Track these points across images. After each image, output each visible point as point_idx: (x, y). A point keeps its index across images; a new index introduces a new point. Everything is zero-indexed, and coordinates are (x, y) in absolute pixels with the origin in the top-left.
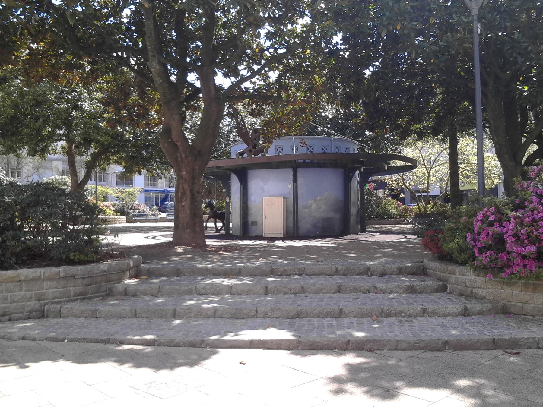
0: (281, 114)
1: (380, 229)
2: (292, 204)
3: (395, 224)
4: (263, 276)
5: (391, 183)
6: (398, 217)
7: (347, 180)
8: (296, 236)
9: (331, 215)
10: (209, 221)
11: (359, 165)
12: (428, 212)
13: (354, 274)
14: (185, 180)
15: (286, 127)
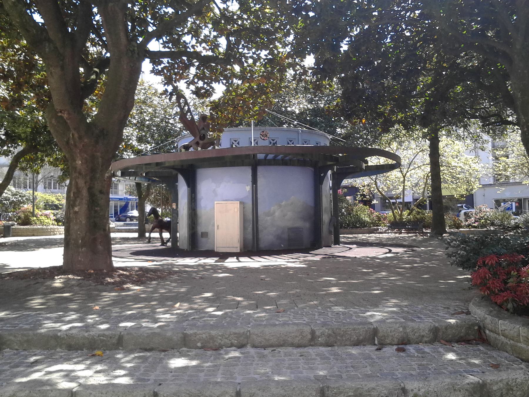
0: (234, 94)
1: (354, 239)
2: (251, 210)
3: (369, 233)
4: (164, 351)
5: (362, 188)
6: (372, 225)
7: (318, 181)
8: (255, 250)
9: (299, 224)
10: (153, 231)
11: (332, 163)
12: (404, 220)
13: (348, 343)
14: (80, 173)
15: (240, 110)
